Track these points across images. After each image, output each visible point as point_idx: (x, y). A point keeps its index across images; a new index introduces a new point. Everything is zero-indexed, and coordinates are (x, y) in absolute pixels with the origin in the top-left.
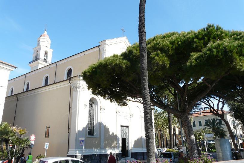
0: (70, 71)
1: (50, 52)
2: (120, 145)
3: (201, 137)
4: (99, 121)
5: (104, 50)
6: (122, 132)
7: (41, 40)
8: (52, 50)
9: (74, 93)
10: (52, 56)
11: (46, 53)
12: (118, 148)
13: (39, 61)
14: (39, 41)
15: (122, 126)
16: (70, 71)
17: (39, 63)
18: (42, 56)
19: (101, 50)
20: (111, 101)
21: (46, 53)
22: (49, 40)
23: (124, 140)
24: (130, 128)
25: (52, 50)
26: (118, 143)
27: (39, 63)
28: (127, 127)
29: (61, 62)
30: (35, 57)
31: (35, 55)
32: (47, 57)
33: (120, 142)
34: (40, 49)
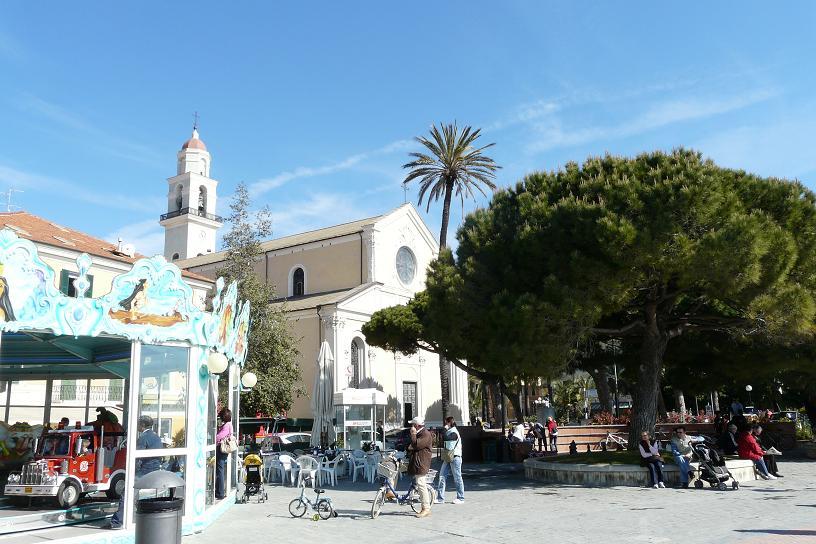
0: (299, 275)
1: (212, 187)
2: (403, 416)
3: (578, 396)
4: (367, 376)
5: (371, 243)
6: (405, 392)
7: (188, 157)
8: (215, 183)
9: (326, 331)
10: (463, 415)
11: (203, 190)
12: (398, 421)
13: (190, 216)
14: (182, 161)
15: (404, 383)
16: (299, 275)
17: (188, 220)
18: (194, 203)
19: (365, 242)
20: (394, 351)
21: (203, 190)
22: (206, 155)
23: (408, 407)
24: (418, 384)
25: (215, 183)
26: (399, 413)
27: (188, 220)
28: (415, 383)
29: (278, 253)
30: (174, 202)
31: (175, 196)
32: (204, 204)
33: (402, 411)
34: (188, 182)
